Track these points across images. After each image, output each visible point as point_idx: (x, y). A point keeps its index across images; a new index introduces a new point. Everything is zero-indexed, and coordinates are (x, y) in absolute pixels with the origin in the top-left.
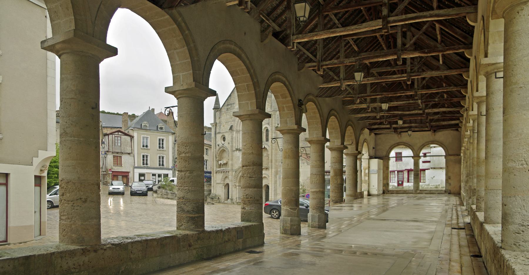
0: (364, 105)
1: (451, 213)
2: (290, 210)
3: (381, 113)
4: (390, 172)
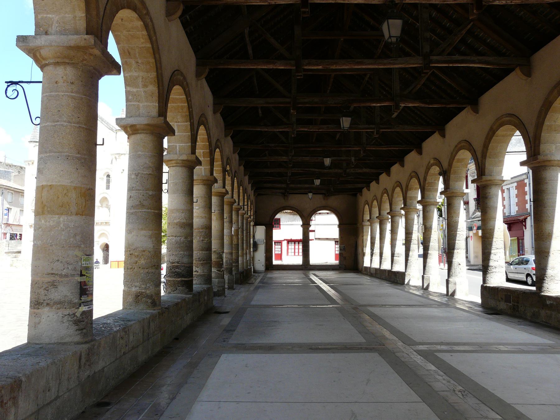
0: (284, 157)
1: (512, 220)
2: (217, 272)
3: (293, 169)
4: (275, 243)
